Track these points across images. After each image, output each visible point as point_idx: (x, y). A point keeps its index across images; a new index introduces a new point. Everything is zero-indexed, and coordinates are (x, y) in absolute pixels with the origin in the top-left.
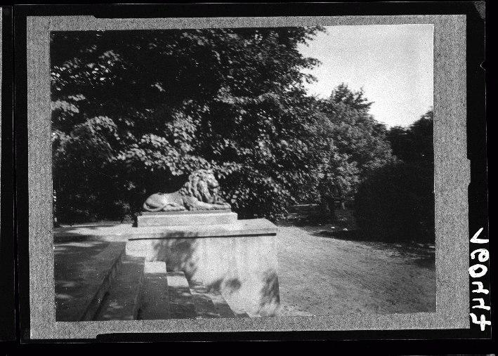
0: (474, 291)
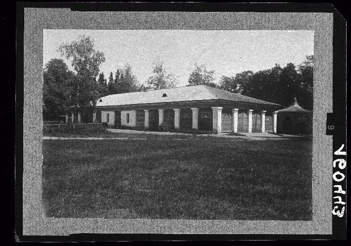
0: (335, 192)
